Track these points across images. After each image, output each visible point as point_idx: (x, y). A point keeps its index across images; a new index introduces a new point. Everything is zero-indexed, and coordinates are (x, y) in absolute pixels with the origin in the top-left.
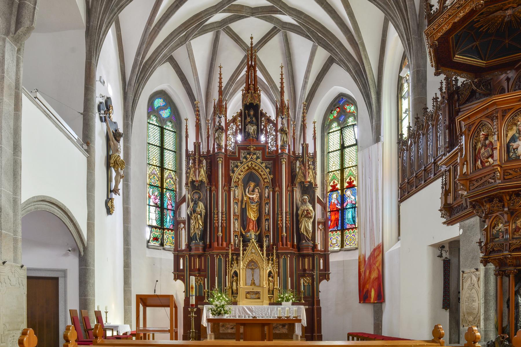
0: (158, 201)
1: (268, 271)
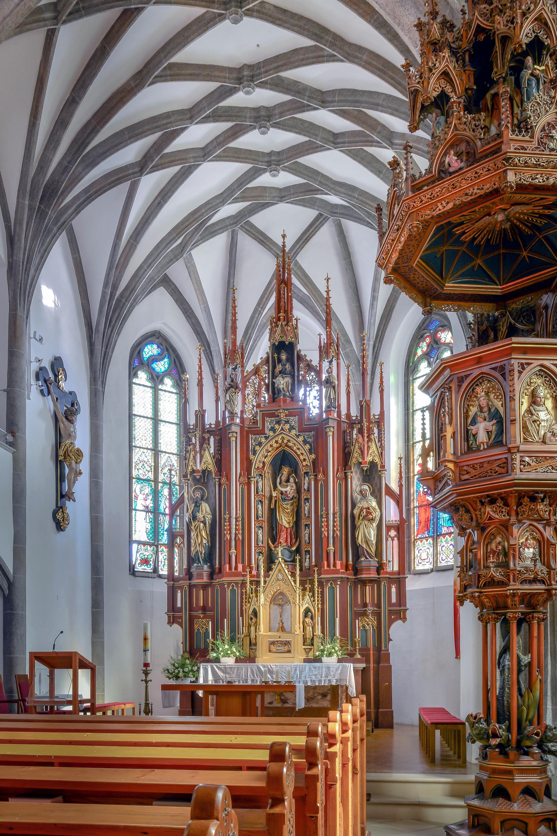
0: (150, 503)
1: (302, 610)
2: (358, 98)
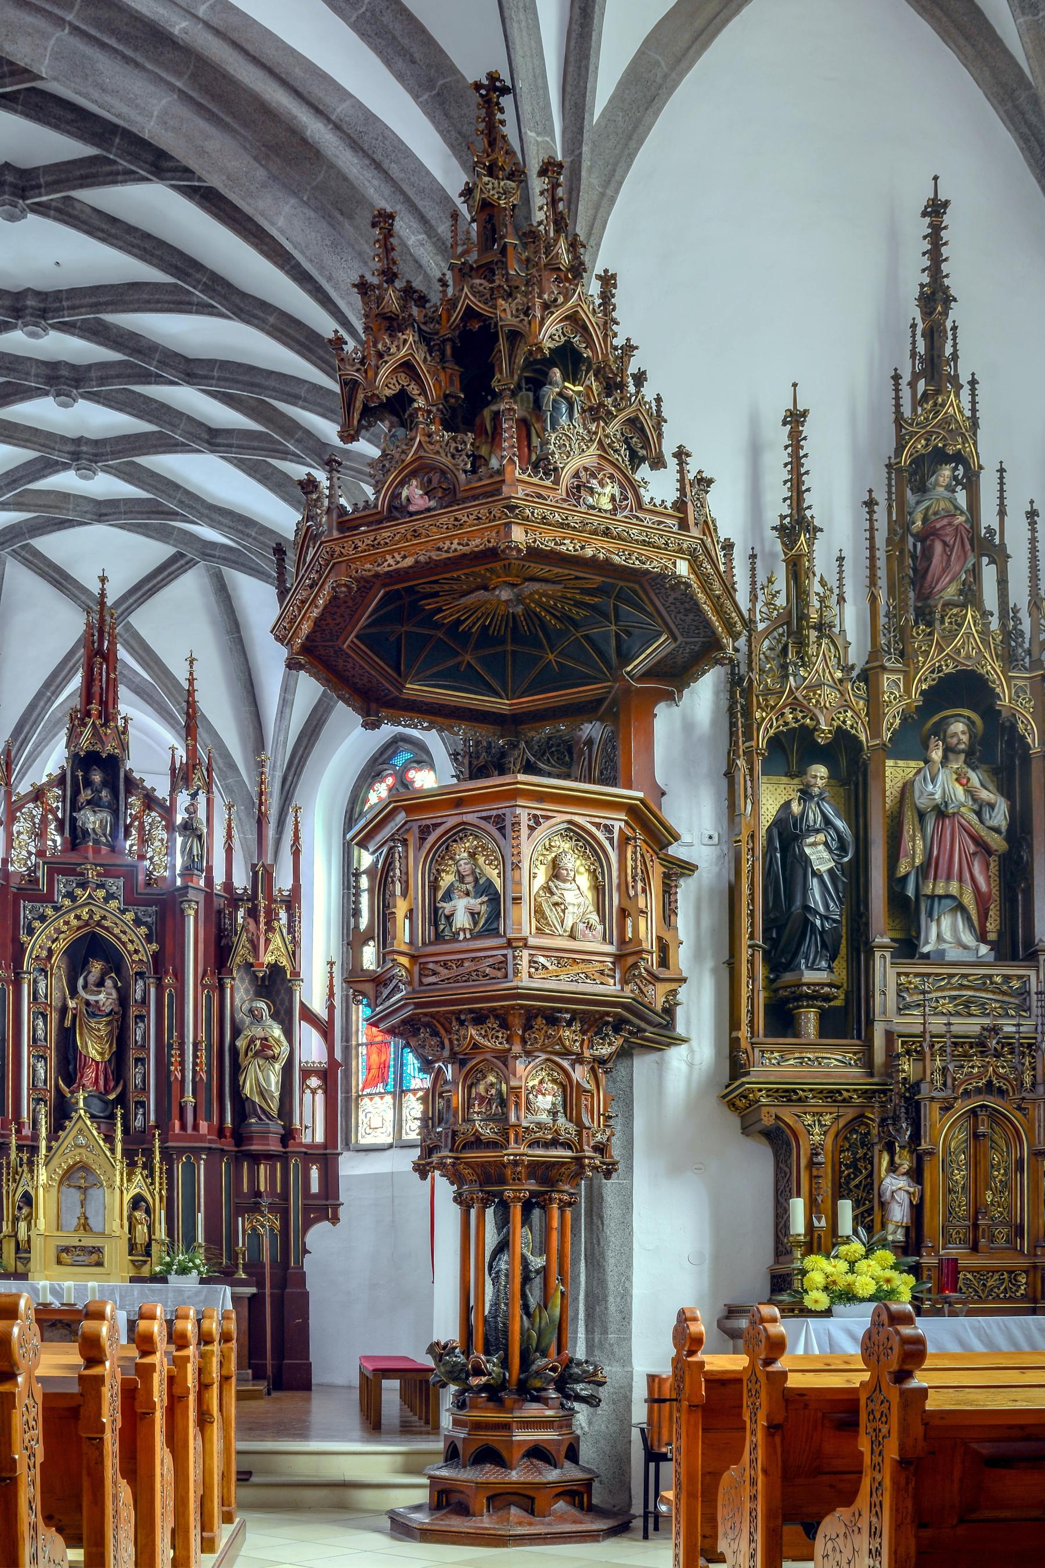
1: (127, 1198)
2: (257, 380)
